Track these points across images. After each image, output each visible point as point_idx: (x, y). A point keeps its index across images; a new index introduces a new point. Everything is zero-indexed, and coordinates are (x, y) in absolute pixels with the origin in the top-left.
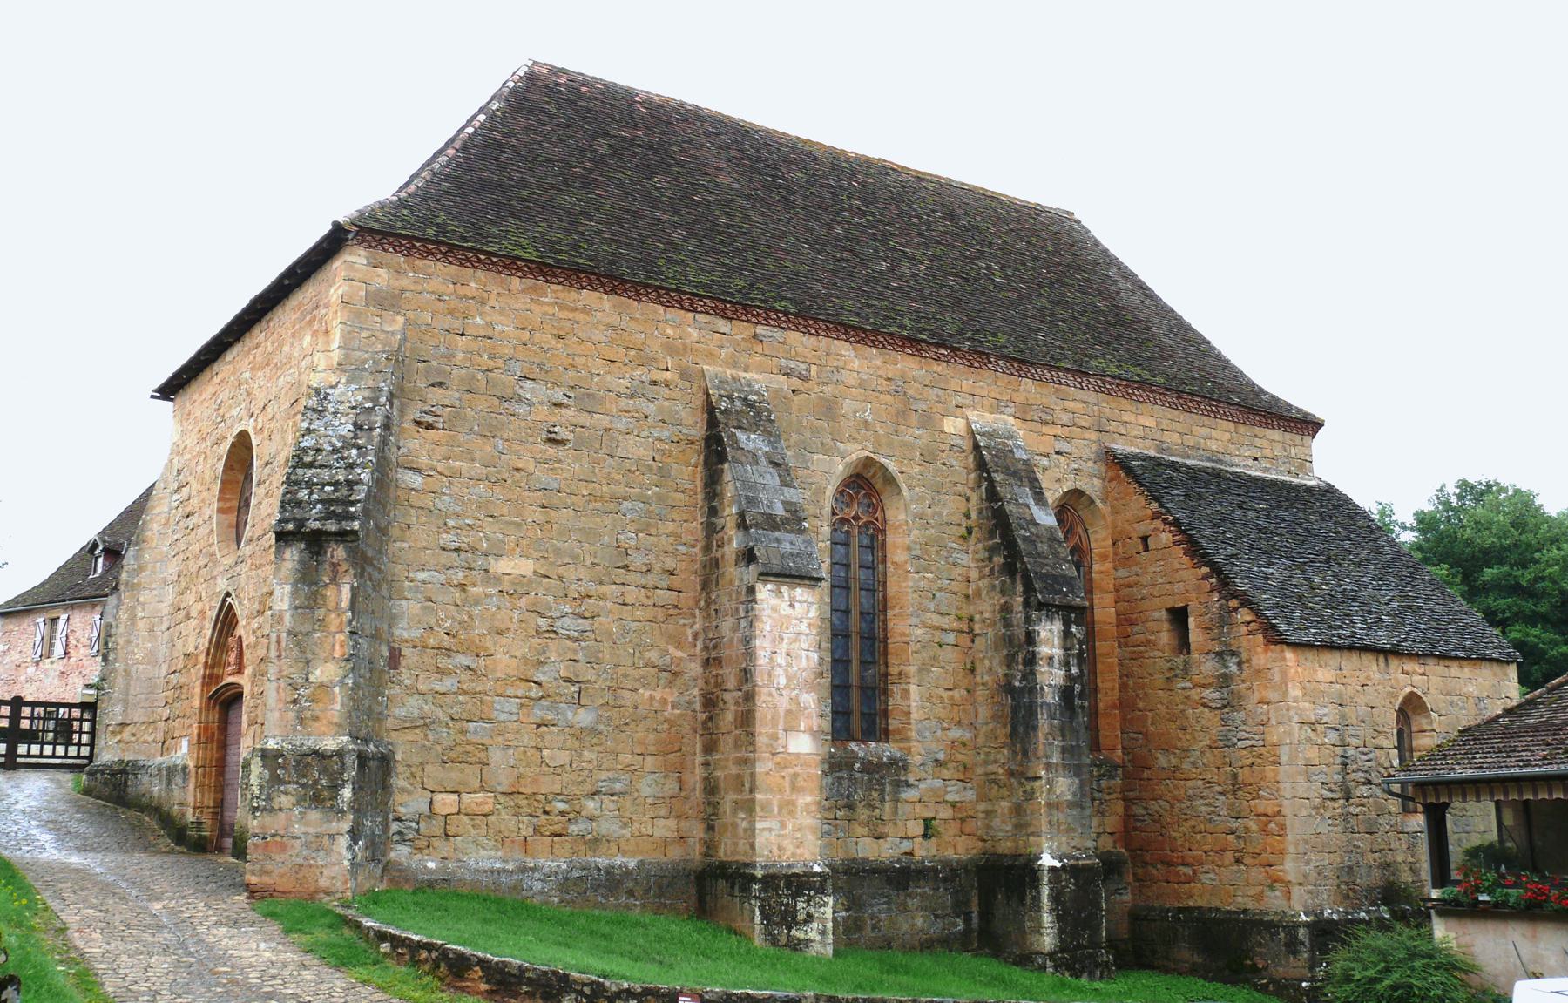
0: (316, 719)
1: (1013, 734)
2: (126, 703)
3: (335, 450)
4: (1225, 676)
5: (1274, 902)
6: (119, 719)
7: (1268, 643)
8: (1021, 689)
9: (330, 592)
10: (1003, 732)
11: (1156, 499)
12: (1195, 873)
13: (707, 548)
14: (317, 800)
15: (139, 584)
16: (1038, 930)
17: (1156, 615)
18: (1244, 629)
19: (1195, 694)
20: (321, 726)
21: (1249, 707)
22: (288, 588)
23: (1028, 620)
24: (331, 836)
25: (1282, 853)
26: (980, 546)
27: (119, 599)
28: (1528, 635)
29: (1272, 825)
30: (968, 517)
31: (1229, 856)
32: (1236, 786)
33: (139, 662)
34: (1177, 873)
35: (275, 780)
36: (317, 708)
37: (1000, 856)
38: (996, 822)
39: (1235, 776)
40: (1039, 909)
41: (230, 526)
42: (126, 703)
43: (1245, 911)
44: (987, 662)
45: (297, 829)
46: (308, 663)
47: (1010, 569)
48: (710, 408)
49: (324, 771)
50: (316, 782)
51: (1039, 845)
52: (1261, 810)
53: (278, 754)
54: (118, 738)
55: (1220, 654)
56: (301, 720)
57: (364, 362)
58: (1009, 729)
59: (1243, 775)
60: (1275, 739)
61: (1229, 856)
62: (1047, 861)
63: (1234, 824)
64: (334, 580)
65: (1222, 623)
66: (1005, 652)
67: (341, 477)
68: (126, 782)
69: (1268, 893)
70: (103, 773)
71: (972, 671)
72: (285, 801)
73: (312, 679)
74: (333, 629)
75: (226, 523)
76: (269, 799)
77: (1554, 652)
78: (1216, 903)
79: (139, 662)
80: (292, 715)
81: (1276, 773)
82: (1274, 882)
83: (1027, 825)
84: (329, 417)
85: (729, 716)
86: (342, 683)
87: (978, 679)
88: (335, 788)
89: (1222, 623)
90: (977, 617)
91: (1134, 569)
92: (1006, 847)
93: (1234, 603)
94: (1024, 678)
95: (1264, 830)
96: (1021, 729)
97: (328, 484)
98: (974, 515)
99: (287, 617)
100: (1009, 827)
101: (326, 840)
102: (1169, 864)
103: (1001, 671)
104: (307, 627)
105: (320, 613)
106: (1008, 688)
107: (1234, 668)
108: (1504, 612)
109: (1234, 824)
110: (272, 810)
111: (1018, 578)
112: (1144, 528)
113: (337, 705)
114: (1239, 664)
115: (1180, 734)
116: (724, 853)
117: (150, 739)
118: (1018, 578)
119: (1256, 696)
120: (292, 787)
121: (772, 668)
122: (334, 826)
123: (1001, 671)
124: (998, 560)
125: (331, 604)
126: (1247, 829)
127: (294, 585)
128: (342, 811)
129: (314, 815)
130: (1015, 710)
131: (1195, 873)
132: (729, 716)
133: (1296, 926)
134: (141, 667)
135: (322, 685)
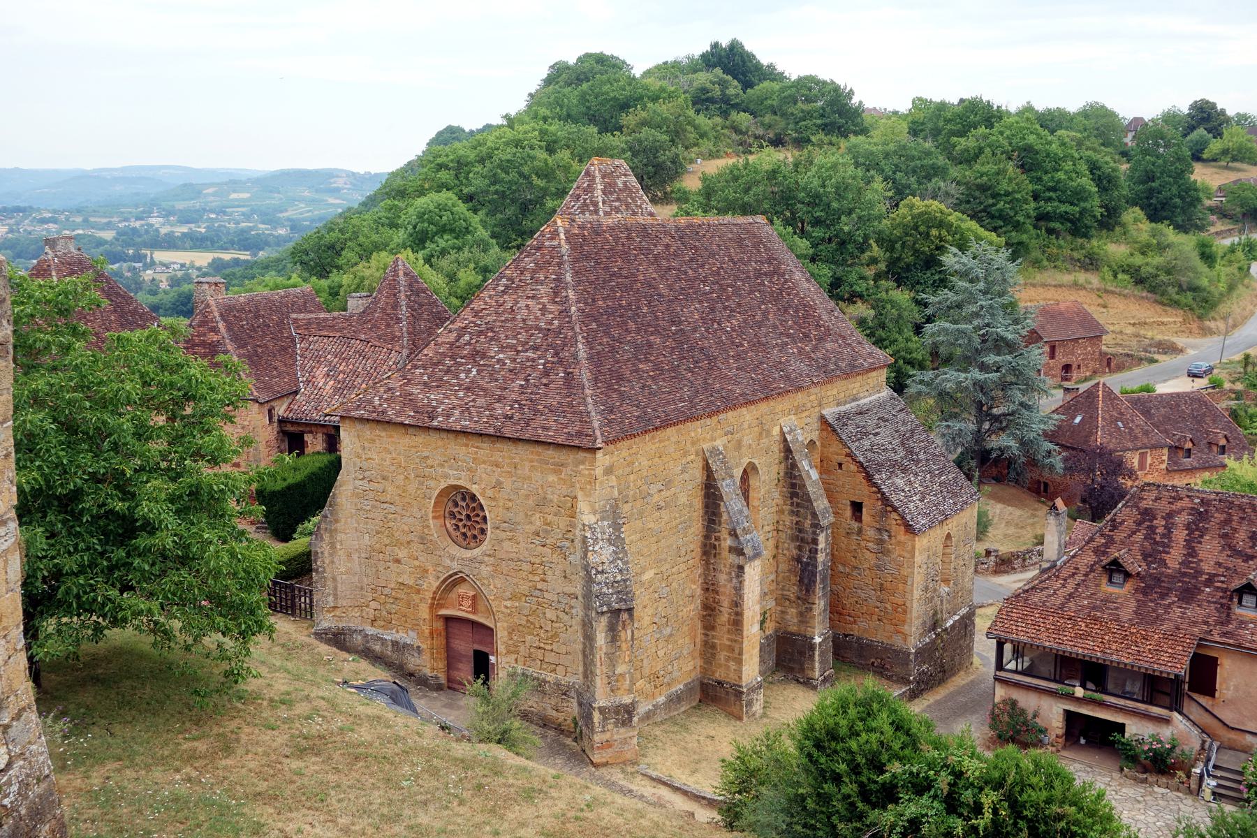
0: (618, 689)
5: (897, 641)
7: (906, 531)
9: (622, 634)
14: (624, 724)
16: (813, 669)
17: (844, 502)
18: (894, 522)
20: (620, 692)
22: (603, 634)
32: (882, 588)
33: (342, 573)
36: (619, 684)
39: (882, 584)
40: (813, 661)
51: (814, 632)
53: (605, 708)
55: (879, 530)
61: (875, 617)
62: (818, 640)
64: (623, 628)
70: (326, 634)
79: (342, 573)
86: (629, 672)
92: (793, 629)
93: (889, 509)
94: (810, 558)
95: (895, 610)
99: (604, 647)
105: (618, 643)
106: (798, 560)
107: (886, 537)
116: (719, 674)
119: (897, 553)
120: (612, 721)
121: (946, 766)
122: (631, 734)
123: (795, 552)
126: (886, 608)
129: (622, 730)
130: (802, 571)
134: (344, 576)
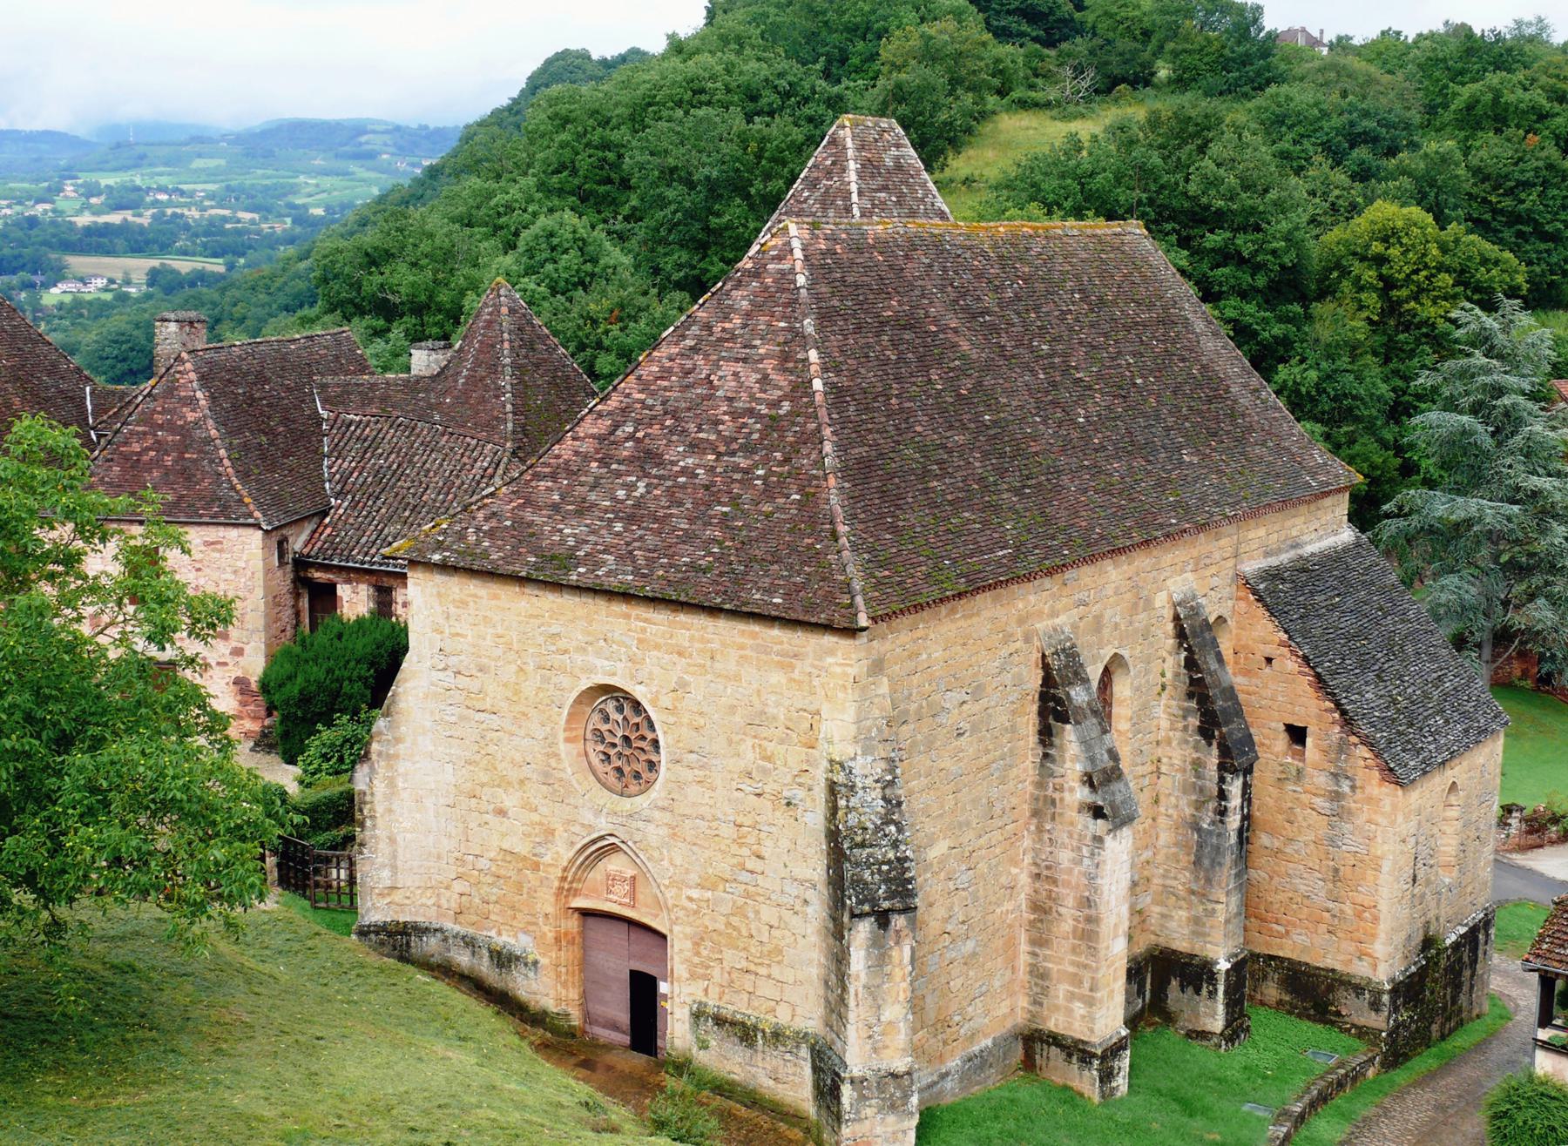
0: (886, 1047)
1: (1197, 862)
2: (394, 868)
3: (877, 829)
4: (1336, 792)
6: (388, 883)
8: (1210, 833)
10: (1186, 859)
11: (1286, 632)
12: (1287, 932)
13: (1040, 785)
14: (893, 1107)
15: (396, 756)
17: (1273, 725)
18: (1362, 763)
19: (1305, 798)
21: (1358, 822)
23: (1222, 780)
24: (904, 1132)
25: (1374, 936)
26: (1174, 703)
27: (372, 769)
28: (1242, 314)
29: (1367, 915)
30: (1163, 675)
31: (1323, 928)
34: (1271, 929)
35: (862, 1098)
37: (1174, 952)
38: (1173, 925)
39: (1336, 871)
41: (579, 755)
42: (394, 868)
43: (1333, 971)
44: (1173, 799)
45: (879, 1130)
46: (879, 1007)
47: (1206, 732)
48: (1046, 667)
49: (899, 1087)
50: (892, 1095)
52: (1359, 900)
54: (388, 900)
55: (1335, 775)
56: (875, 1050)
57: (869, 731)
58: (1192, 858)
59: (1345, 871)
60: (1379, 853)
61: (1323, 928)
63: (1331, 905)
64: (897, 943)
65: (1340, 750)
66: (1194, 797)
67: (891, 855)
68: (408, 944)
69: (1356, 961)
71: (1157, 802)
72: (869, 1112)
73: (883, 1018)
74: (898, 979)
75: (575, 752)
76: (858, 1112)
77: (1266, 334)
78: (1308, 960)
80: (868, 1047)
81: (1376, 878)
82: (1361, 955)
83: (1204, 935)
84: (861, 793)
85: (1067, 926)
87: (1162, 809)
88: (906, 1097)
89: (1340, 750)
90: (1165, 760)
91: (1254, 680)
95: (1359, 916)
96: (1206, 862)
97: (884, 863)
98: (1169, 675)
100: (1186, 931)
101: (900, 1135)
102: (1263, 920)
103: (1188, 811)
104: (878, 981)
105: (888, 969)
107: (1346, 789)
108: (1221, 284)
109: (1331, 905)
110: (860, 1120)
111: (1215, 743)
112: (1270, 650)
113: (901, 1037)
114: (1353, 788)
115: (1287, 825)
117: (430, 902)
118: (1215, 743)
123: (1188, 811)
124: (1194, 721)
125: (896, 960)
127: (867, 950)
128: (912, 1113)
129: (891, 1119)
130: (1200, 846)
131: (1287, 932)
132: (1067, 926)
133: (1380, 993)
134: (409, 836)
135: (890, 1023)
